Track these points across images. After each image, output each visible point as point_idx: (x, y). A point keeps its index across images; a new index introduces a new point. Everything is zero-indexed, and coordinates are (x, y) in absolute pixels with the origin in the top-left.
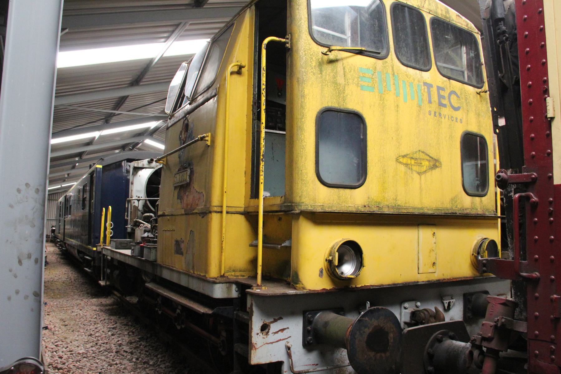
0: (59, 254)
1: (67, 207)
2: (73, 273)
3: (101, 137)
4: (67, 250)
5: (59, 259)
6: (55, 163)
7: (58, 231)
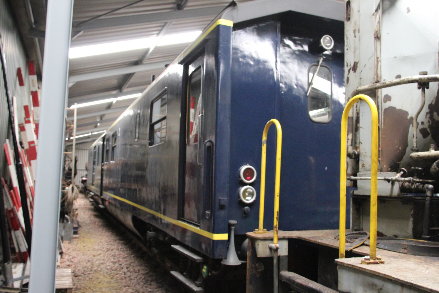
0: (92, 210)
1: (107, 151)
2: (120, 248)
3: (117, 102)
4: (105, 209)
5: (93, 218)
6: (80, 128)
7: (91, 182)
